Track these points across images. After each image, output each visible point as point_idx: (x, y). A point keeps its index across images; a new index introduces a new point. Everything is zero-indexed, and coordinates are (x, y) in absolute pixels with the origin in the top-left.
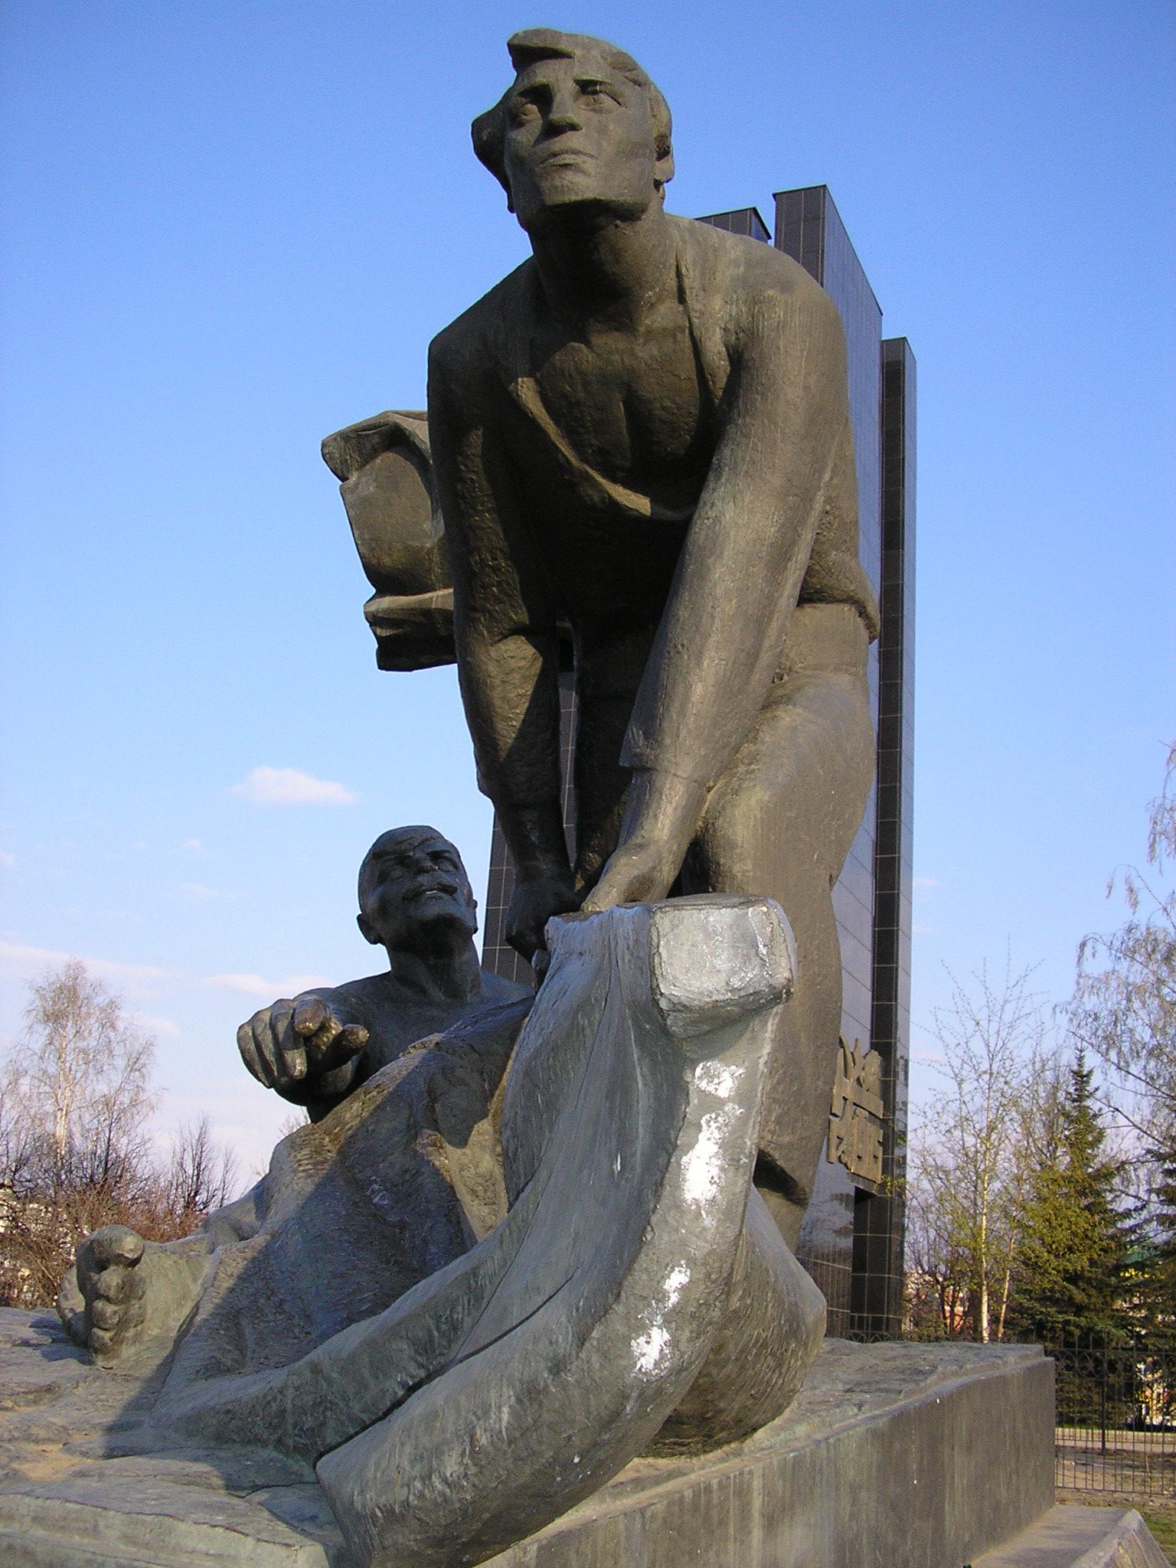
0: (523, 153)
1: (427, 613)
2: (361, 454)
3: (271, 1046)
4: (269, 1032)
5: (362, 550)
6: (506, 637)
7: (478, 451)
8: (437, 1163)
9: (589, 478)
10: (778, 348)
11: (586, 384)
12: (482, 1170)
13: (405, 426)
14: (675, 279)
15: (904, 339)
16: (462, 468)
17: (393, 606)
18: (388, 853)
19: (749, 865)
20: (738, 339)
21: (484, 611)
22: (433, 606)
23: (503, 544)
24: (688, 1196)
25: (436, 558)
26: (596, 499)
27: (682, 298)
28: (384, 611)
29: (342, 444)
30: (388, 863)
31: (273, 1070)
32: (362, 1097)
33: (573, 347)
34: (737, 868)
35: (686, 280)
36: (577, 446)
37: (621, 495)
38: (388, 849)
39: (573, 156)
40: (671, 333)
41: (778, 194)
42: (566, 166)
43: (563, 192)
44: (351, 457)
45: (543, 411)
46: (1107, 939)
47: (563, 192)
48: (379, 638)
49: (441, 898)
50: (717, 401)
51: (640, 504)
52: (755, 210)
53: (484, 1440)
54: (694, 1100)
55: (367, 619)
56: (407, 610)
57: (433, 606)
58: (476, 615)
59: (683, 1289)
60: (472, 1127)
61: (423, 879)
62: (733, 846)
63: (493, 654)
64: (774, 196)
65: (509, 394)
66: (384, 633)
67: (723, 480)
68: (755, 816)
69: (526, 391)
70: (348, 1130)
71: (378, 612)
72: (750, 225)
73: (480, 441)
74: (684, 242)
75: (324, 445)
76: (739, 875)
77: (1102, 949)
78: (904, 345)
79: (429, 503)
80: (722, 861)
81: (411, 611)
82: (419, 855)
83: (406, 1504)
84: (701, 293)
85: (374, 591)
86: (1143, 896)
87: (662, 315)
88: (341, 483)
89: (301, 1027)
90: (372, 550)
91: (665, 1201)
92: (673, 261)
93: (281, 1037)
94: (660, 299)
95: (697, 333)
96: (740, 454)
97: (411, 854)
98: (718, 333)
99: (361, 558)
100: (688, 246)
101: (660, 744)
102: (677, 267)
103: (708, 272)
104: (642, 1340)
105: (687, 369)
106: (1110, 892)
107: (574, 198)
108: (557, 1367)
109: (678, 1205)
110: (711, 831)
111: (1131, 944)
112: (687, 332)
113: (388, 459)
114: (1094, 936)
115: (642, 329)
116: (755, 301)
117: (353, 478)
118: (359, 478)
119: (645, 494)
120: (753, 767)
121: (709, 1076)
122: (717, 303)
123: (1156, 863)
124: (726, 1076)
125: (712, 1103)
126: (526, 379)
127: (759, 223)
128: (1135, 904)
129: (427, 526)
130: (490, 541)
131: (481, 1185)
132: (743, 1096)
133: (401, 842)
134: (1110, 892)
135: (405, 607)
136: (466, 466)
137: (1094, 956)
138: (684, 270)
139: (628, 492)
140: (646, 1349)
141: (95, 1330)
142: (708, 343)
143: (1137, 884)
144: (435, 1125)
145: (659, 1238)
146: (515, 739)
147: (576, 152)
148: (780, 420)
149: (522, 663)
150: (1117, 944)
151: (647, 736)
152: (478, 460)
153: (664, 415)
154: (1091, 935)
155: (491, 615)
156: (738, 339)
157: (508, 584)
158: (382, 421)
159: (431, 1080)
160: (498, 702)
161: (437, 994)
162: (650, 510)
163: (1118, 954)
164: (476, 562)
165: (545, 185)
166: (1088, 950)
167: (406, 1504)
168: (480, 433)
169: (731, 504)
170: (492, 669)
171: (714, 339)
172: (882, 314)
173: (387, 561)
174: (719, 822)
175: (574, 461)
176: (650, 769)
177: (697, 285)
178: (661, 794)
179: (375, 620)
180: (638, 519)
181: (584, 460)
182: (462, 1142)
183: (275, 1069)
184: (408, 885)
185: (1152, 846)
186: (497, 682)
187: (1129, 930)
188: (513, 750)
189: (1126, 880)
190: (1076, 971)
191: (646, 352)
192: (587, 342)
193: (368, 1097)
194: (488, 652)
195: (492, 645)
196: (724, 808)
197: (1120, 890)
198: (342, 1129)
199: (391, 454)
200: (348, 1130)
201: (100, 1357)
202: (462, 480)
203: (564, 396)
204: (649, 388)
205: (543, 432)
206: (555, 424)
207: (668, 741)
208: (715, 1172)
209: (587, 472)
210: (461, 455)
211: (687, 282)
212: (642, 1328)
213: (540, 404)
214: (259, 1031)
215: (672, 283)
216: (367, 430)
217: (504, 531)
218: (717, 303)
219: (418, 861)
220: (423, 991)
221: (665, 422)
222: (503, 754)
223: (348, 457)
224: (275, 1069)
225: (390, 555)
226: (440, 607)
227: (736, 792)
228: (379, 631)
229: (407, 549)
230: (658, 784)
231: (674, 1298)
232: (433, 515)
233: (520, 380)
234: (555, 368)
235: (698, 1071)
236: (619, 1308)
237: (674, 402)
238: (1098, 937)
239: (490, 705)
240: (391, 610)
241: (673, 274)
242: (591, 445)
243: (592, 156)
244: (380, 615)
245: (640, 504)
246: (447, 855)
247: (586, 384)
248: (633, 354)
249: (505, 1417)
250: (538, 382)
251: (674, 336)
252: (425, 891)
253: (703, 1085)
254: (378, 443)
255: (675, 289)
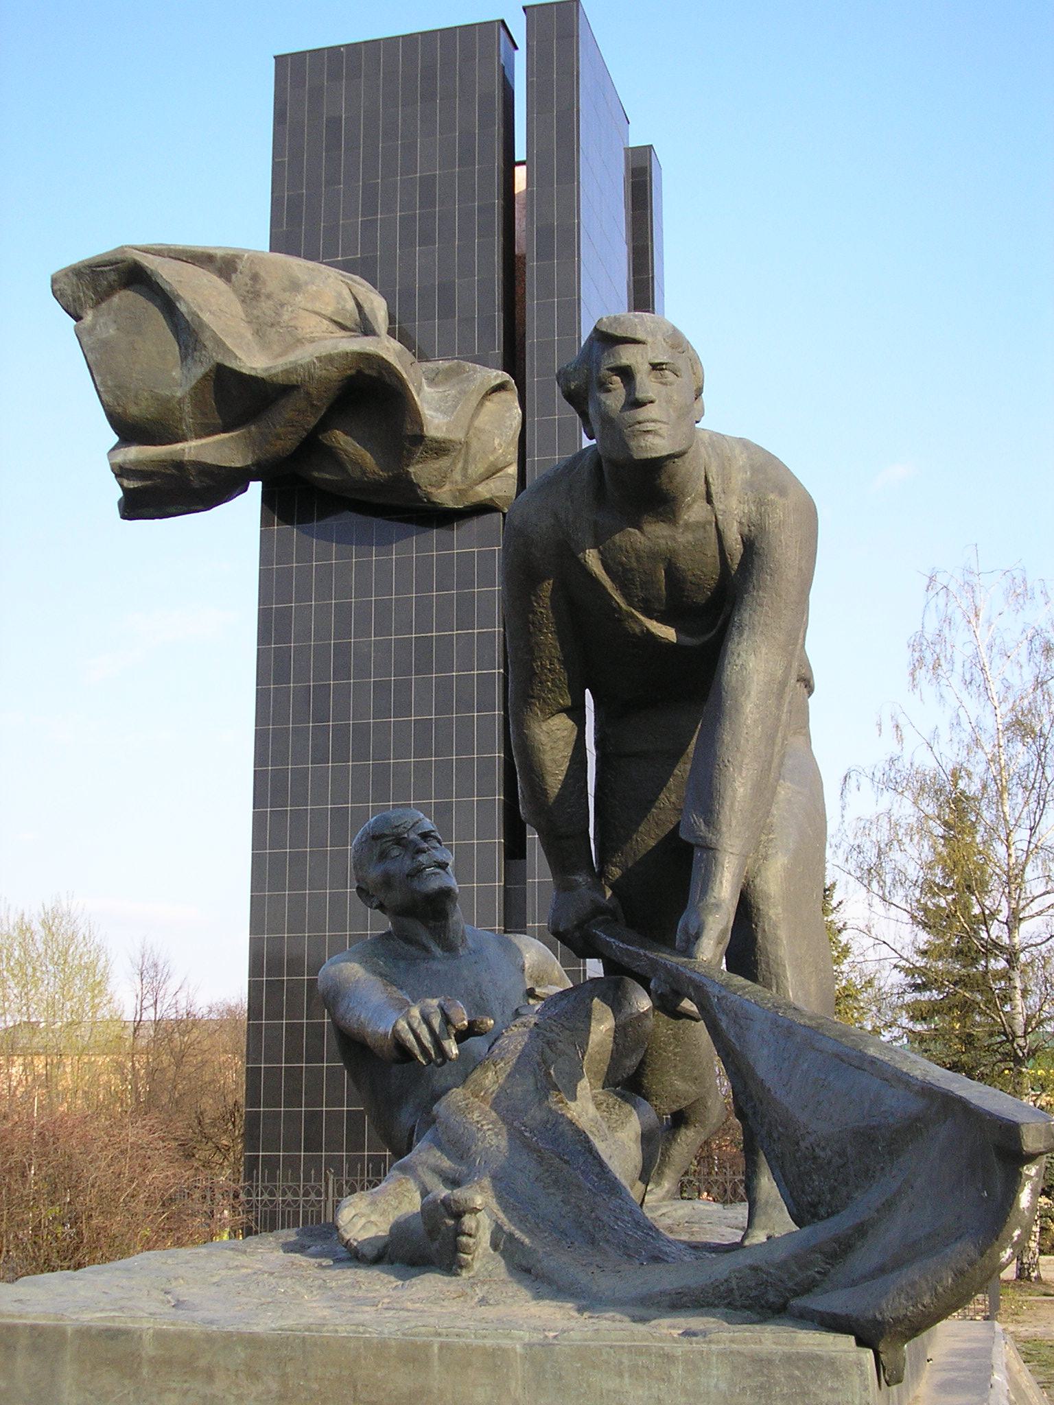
0: (612, 415)
1: (179, 465)
2: (96, 292)
3: (428, 1036)
4: (424, 1026)
5: (105, 397)
6: (553, 715)
7: (548, 594)
8: (569, 1115)
9: (632, 616)
10: (781, 541)
11: (638, 558)
12: (590, 1116)
13: (146, 264)
14: (705, 486)
15: (651, 146)
16: (535, 604)
17: (141, 457)
18: (387, 836)
19: (780, 910)
20: (750, 531)
21: (539, 698)
22: (186, 458)
23: (559, 654)
24: (1021, 1207)
25: (187, 408)
26: (637, 630)
27: (709, 499)
28: (131, 462)
29: (74, 280)
30: (389, 844)
31: (431, 1054)
32: (493, 1067)
33: (630, 532)
34: (771, 912)
35: (712, 487)
36: (627, 597)
37: (655, 628)
38: (387, 832)
39: (653, 424)
40: (702, 525)
41: (528, 7)
42: (648, 432)
43: (647, 451)
44: (84, 293)
45: (603, 572)
46: (869, 772)
47: (647, 451)
48: (124, 489)
49: (439, 873)
50: (733, 572)
51: (668, 633)
52: (503, 22)
53: (940, 1290)
54: (1024, 1177)
55: (113, 470)
56: (158, 461)
57: (186, 459)
58: (533, 700)
59: (1019, 1236)
60: (576, 1085)
61: (423, 858)
62: (768, 897)
63: (544, 728)
64: (525, 9)
65: (578, 560)
66: (132, 484)
67: (745, 636)
68: (781, 876)
69: (592, 558)
70: (492, 1094)
71: (125, 463)
72: (499, 39)
73: (550, 587)
74: (709, 457)
75: (54, 281)
76: (773, 917)
77: (866, 783)
78: (650, 153)
79: (177, 348)
80: (761, 907)
81: (163, 463)
82: (413, 836)
83: (905, 1315)
84: (723, 496)
85: (116, 439)
86: (907, 731)
87: (695, 512)
88: (75, 323)
89: (459, 1024)
90: (117, 398)
91: (1014, 1209)
92: (703, 474)
93: (437, 1030)
94: (694, 501)
95: (721, 527)
96: (756, 618)
97: (406, 836)
98: (735, 526)
99: (103, 406)
100: (713, 459)
101: (719, 831)
102: (706, 477)
103: (726, 479)
104: (1003, 1252)
105: (712, 550)
106: (880, 730)
107: (654, 455)
108: (972, 1263)
109: (1018, 1209)
110: (752, 887)
111: (892, 775)
112: (714, 524)
113: (126, 299)
114: (856, 768)
115: (681, 522)
116: (761, 503)
117: (89, 317)
118: (95, 316)
119: (672, 626)
120: (771, 836)
121: (1028, 1169)
122: (734, 502)
123: (917, 691)
124: (1033, 1169)
125: (1029, 1177)
126: (591, 550)
127: (508, 39)
128: (900, 739)
129: (176, 373)
130: (550, 652)
131: (594, 1127)
132: (1037, 1174)
133: (396, 827)
134: (880, 730)
135: (155, 459)
136: (538, 603)
137: (859, 789)
138: (711, 480)
139: (660, 625)
140: (1004, 1255)
141: (462, 1255)
142: (729, 533)
143: (902, 721)
144: (555, 1087)
145: (1012, 1220)
146: (560, 789)
147: (654, 421)
148: (783, 594)
149: (565, 733)
150: (878, 775)
151: (707, 823)
152: (547, 600)
153: (693, 579)
154: (852, 769)
155: (544, 701)
156: (750, 531)
157: (560, 680)
158: (119, 257)
159: (542, 1052)
160: (548, 763)
161: (438, 951)
162: (675, 638)
163: (881, 786)
164: (537, 666)
165: (633, 444)
166: (852, 783)
167: (905, 1315)
168: (551, 581)
169: (753, 655)
170: (543, 738)
171: (733, 530)
172: (629, 123)
173: (133, 410)
174: (757, 881)
175: (623, 606)
176: (712, 849)
177: (720, 490)
178: (723, 867)
179: (121, 472)
180: (668, 645)
181: (630, 604)
182: (574, 1098)
183: (433, 1053)
184: (407, 865)
185: (912, 674)
186: (548, 748)
187: (892, 761)
188: (559, 796)
189: (892, 717)
190: (840, 803)
191: (683, 538)
192: (640, 529)
193: (498, 1067)
194: (540, 726)
195: (543, 721)
196: (759, 870)
197: (888, 726)
198: (485, 1093)
199: (129, 292)
200: (492, 1094)
201: (464, 1271)
202: (535, 613)
203: (621, 564)
204: (683, 563)
205: (604, 588)
206: (612, 580)
207: (724, 829)
208: (1029, 1198)
209: (633, 614)
210: (534, 595)
211: (713, 489)
212: (1004, 1249)
213: (601, 567)
214: (415, 1025)
215: (702, 488)
216: (99, 266)
217: (561, 645)
218: (734, 502)
219: (412, 841)
220: (426, 949)
221: (694, 584)
222: (552, 800)
223: (82, 295)
224: (433, 1053)
225: (136, 404)
226: (194, 459)
227: (765, 858)
228: (126, 483)
229: (156, 398)
230: (720, 860)
231: (1016, 1239)
232: (182, 362)
233: (587, 551)
234: (614, 545)
235: (1025, 1168)
236: (997, 1243)
237: (702, 571)
238: (861, 770)
239: (541, 765)
240: (139, 462)
241: (703, 480)
242: (637, 596)
243: (665, 423)
244: (127, 466)
245: (668, 633)
246: (433, 834)
247: (638, 558)
248: (674, 539)
249: (950, 1280)
250: (600, 552)
251: (704, 528)
252: (425, 868)
253: (1027, 1172)
254: (114, 281)
255: (704, 493)
